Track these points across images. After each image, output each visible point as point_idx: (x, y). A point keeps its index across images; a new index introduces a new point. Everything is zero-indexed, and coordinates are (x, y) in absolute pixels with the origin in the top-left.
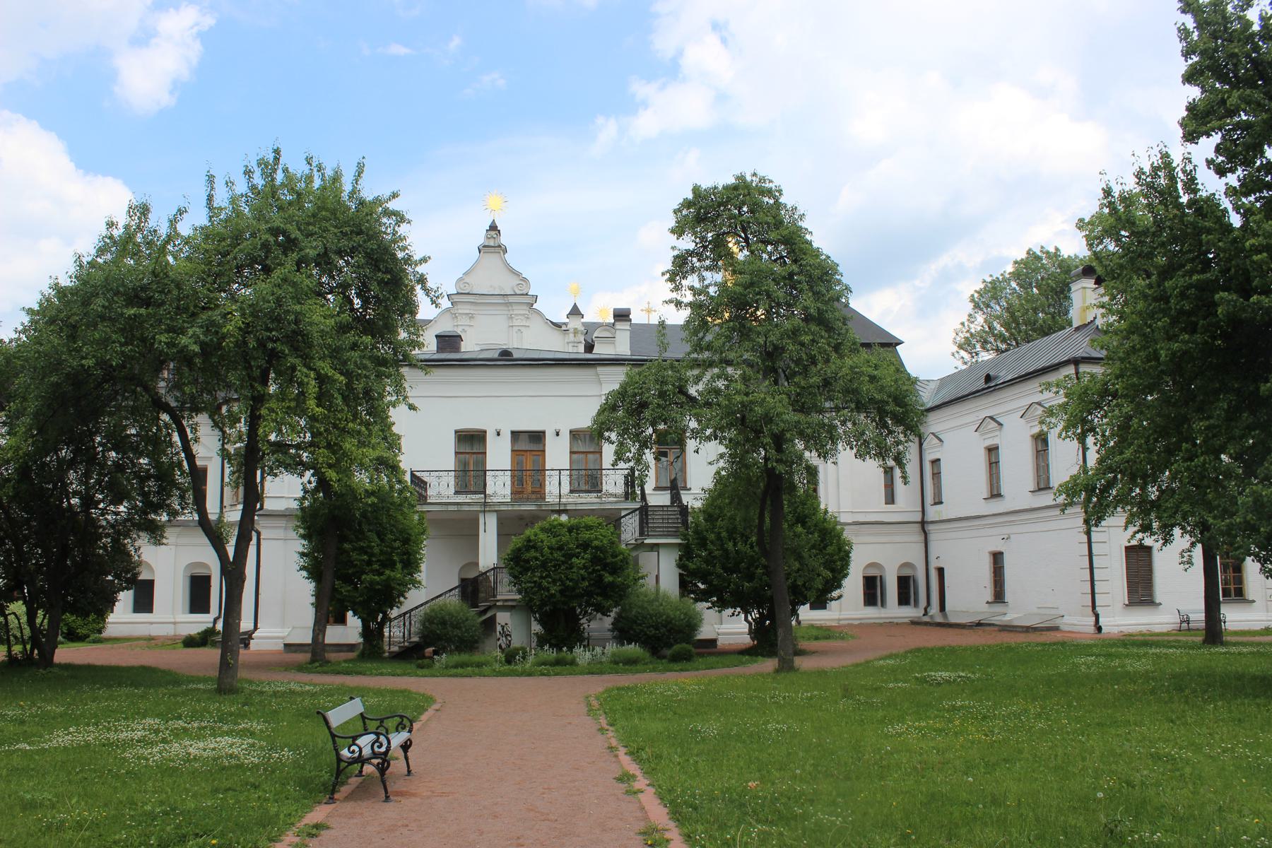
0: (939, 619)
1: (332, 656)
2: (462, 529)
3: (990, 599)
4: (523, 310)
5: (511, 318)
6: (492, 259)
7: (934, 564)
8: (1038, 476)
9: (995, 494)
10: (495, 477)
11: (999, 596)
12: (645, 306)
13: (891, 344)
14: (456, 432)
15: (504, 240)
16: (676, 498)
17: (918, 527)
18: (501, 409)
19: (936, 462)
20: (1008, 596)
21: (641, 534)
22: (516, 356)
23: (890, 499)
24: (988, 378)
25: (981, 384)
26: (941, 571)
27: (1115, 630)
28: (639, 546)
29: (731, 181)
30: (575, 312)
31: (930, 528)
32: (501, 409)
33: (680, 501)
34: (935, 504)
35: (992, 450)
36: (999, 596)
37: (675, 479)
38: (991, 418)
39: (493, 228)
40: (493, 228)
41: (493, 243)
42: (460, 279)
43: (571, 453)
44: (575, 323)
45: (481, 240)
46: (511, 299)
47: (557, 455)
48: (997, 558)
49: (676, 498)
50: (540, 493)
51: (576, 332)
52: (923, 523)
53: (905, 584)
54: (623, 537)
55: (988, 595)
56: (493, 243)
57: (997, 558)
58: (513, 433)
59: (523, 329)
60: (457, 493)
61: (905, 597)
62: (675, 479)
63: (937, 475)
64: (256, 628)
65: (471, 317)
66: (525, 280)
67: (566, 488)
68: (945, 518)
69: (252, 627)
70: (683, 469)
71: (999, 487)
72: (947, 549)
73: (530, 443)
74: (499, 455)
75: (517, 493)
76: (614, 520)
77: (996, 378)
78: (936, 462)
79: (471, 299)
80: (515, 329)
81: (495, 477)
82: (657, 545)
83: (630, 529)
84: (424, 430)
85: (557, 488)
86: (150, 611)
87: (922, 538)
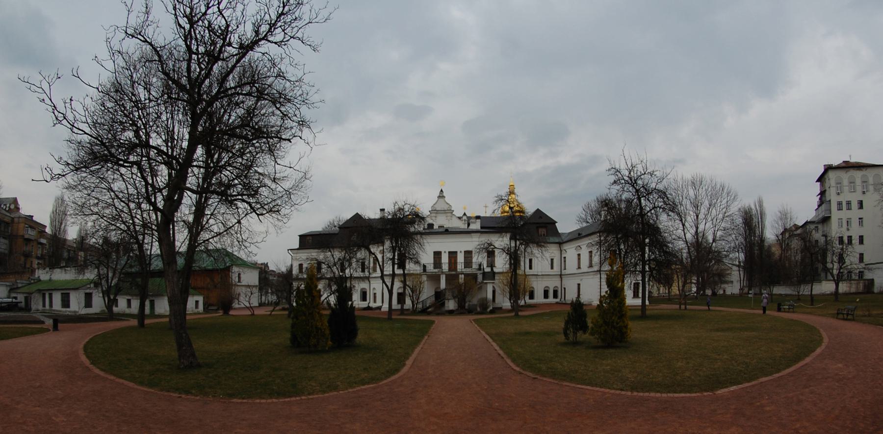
6: (441, 200)
13: (554, 223)
15: (445, 194)
16: (492, 269)
18: (445, 245)
23: (552, 268)
30: (465, 214)
35: (579, 255)
41: (441, 196)
47: (461, 258)
48: (579, 285)
49: (492, 269)
56: (441, 196)
57: (579, 285)
61: (555, 296)
74: (445, 259)
75: (450, 269)
83: (480, 278)
85: (460, 267)
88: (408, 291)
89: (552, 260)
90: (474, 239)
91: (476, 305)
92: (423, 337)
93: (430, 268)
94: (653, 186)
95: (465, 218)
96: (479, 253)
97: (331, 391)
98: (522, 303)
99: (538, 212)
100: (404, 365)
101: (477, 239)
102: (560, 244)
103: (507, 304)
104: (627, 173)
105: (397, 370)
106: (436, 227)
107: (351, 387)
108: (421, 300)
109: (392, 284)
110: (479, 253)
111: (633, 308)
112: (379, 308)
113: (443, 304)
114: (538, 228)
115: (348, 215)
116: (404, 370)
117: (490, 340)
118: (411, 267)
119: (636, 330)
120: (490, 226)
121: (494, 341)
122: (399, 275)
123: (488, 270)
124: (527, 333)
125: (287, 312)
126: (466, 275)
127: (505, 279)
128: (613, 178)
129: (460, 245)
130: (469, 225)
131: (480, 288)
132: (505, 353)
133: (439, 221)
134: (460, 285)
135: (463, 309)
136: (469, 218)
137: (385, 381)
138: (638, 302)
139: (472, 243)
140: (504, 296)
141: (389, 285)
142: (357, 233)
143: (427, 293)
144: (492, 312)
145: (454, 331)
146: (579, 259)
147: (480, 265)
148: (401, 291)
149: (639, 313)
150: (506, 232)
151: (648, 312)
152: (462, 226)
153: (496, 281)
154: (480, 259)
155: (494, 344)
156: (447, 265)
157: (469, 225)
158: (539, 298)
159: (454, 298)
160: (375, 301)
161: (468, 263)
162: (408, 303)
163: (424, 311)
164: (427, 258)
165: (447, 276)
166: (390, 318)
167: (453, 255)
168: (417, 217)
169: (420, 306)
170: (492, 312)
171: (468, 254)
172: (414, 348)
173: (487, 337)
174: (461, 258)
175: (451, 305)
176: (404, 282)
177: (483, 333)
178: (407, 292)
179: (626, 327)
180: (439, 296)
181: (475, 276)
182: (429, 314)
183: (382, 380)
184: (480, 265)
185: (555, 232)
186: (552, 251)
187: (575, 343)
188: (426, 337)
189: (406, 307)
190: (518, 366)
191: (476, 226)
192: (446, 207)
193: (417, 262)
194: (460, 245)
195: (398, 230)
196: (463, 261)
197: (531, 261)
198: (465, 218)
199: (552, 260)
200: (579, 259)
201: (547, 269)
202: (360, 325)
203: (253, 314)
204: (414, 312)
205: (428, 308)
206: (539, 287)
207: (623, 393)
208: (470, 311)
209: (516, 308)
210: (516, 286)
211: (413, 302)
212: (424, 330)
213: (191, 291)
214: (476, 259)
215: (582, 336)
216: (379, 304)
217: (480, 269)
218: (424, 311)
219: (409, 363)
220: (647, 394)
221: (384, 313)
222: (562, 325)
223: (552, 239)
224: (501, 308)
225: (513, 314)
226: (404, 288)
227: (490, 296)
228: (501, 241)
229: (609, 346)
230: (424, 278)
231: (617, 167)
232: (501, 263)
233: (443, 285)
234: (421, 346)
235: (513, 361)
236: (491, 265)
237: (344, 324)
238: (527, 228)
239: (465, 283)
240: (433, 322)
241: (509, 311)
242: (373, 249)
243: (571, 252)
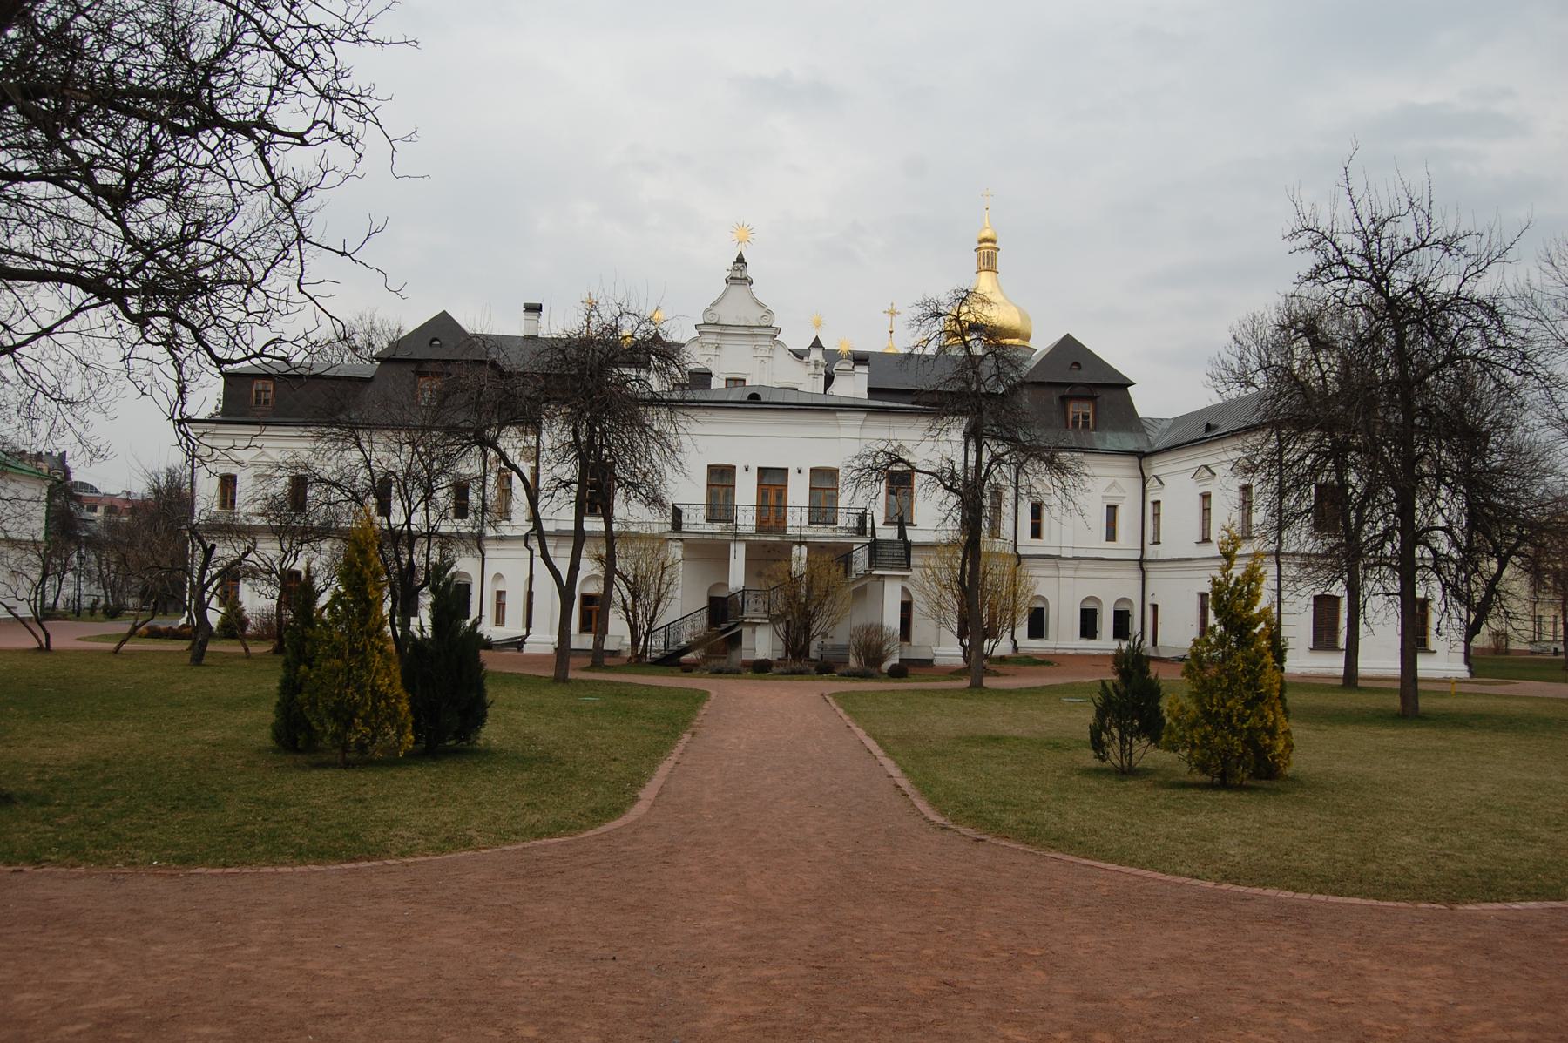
1: (608, 661)
2: (712, 553)
4: (766, 342)
6: (738, 290)
7: (1149, 600)
12: (887, 307)
13: (1123, 385)
15: (751, 272)
16: (902, 534)
18: (747, 445)
19: (1157, 503)
23: (1111, 535)
24: (1209, 428)
25: (1201, 433)
26: (1155, 607)
27: (1298, 671)
28: (867, 575)
30: (817, 343)
31: (1147, 566)
32: (747, 445)
35: (1206, 497)
39: (740, 259)
40: (740, 259)
41: (739, 275)
42: (708, 310)
46: (756, 331)
47: (798, 493)
49: (902, 534)
50: (780, 527)
53: (1122, 619)
56: (739, 275)
61: (1121, 630)
63: (1157, 516)
66: (769, 312)
67: (805, 522)
69: (524, 632)
73: (772, 480)
74: (746, 492)
75: (761, 528)
77: (1216, 427)
78: (1157, 503)
79: (718, 329)
83: (861, 559)
85: (796, 520)
88: (621, 591)
89: (1112, 510)
90: (844, 432)
91: (847, 648)
92: (676, 736)
93: (696, 519)
94: (1447, 286)
95: (816, 355)
96: (858, 482)
97: (455, 848)
98: (1003, 647)
99: (1068, 343)
100: (635, 799)
101: (855, 433)
102: (1141, 456)
103: (949, 650)
104: (1359, 246)
105: (618, 811)
106: (717, 383)
107: (506, 841)
108: (660, 622)
109: (574, 568)
110: (858, 482)
111: (1311, 684)
112: (517, 644)
113: (736, 641)
114: (1064, 400)
115: (411, 318)
116: (636, 812)
117: (878, 752)
118: (629, 512)
119: (1308, 750)
120: (900, 390)
121: (890, 754)
122: (594, 536)
123: (888, 534)
124: (997, 740)
125: (184, 645)
126: (816, 548)
127: (948, 567)
128: (1310, 261)
129: (799, 448)
130: (829, 380)
131: (860, 593)
132: (916, 784)
133: (727, 363)
134: (795, 581)
135: (800, 659)
136: (832, 356)
137: (591, 833)
138: (1333, 664)
139: (843, 444)
140: (942, 622)
141: (563, 567)
142: (449, 386)
143: (682, 604)
144: (899, 672)
145: (766, 727)
146: (1206, 511)
147: (862, 519)
148: (594, 589)
149: (1395, 703)
150: (961, 413)
151: (1423, 703)
152: (809, 383)
153: (915, 574)
154: (862, 499)
155: (889, 764)
156: (753, 512)
157: (829, 380)
158: (1064, 636)
159: (774, 620)
160: (499, 620)
161: (822, 511)
162: (618, 631)
163: (671, 660)
164: (687, 489)
165: (750, 547)
166: (561, 678)
168: (655, 350)
169: (657, 643)
170: (899, 672)
171: (824, 479)
172: (654, 765)
173: (871, 743)
174: (798, 493)
175: (762, 643)
176: (609, 561)
177: (861, 733)
178: (616, 595)
179: (1272, 732)
180: (722, 613)
181: (843, 555)
182: (688, 669)
183: (582, 828)
184: (862, 519)
185: (1126, 418)
186: (1103, 481)
187: (1127, 772)
188: (687, 737)
189: (609, 644)
190: (943, 813)
191: (852, 386)
193: (654, 500)
194: (799, 448)
195: (599, 388)
197: (1037, 511)
198: (816, 355)
199: (1112, 510)
200: (1206, 511)
201: (1095, 542)
202: (491, 692)
203: (45, 649)
204: (638, 660)
205: (685, 650)
206: (1064, 598)
207: (1195, 882)
208: (826, 668)
209: (977, 666)
210: (978, 600)
211: (633, 628)
212: (678, 718)
213: (1398, 685)
214: (849, 500)
215: (1146, 753)
216: (513, 627)
217: (861, 530)
218: (671, 660)
219: (648, 794)
220: (1257, 890)
221: (537, 659)
222: (1088, 716)
223: (1112, 440)
224: (928, 663)
225: (965, 683)
226: (609, 582)
227: (892, 620)
228: (936, 446)
229: (1224, 782)
230: (676, 551)
231: (1324, 225)
232: (933, 516)
233: (737, 577)
234: (674, 758)
235: (934, 802)
236: (901, 520)
237: (448, 687)
238: (1022, 402)
239: (811, 574)
240: (703, 696)
241: (956, 673)
242: (512, 443)
243: (1178, 482)
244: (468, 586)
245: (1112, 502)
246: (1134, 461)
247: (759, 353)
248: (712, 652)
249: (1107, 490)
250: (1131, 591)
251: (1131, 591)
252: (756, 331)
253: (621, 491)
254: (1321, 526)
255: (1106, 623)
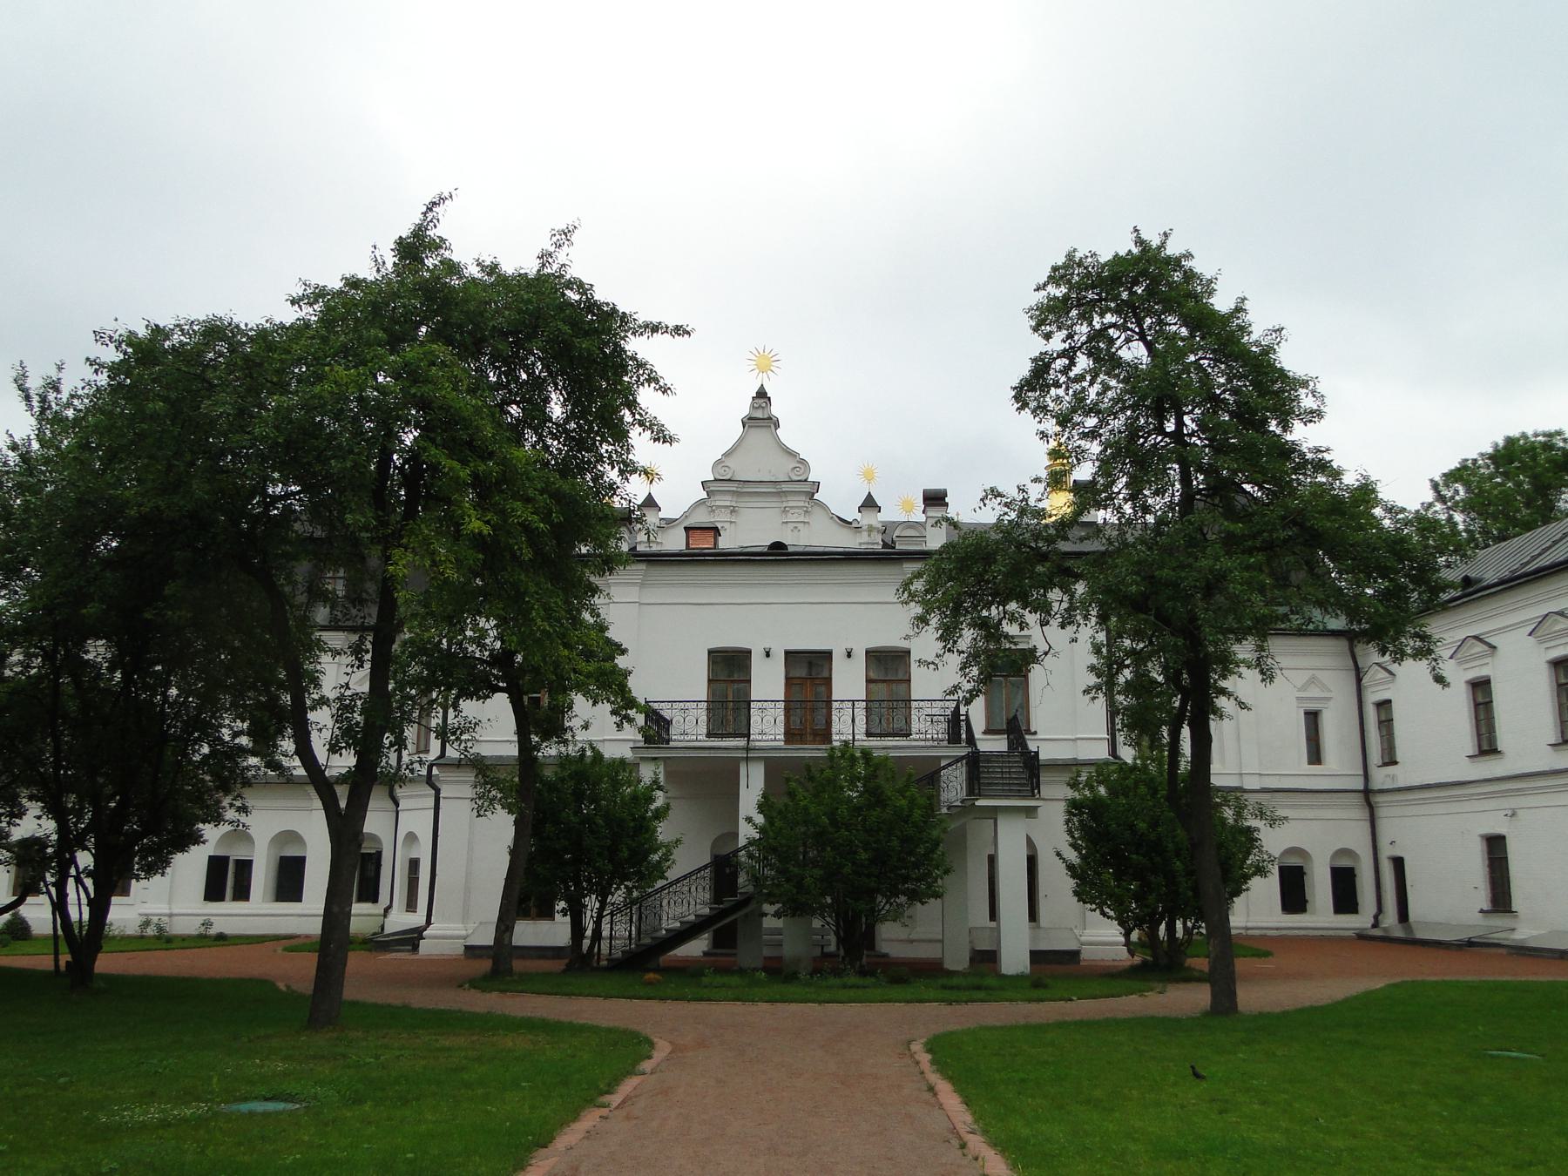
0: (1398, 933)
1: (518, 965)
2: (711, 780)
3: (1486, 906)
4: (801, 502)
5: (785, 511)
6: (759, 435)
7: (1386, 852)
8: (1479, 735)
9: (1487, 746)
10: (762, 710)
11: (1501, 898)
14: (710, 652)
15: (776, 410)
17: (1358, 799)
20: (1517, 904)
21: (970, 791)
22: (791, 549)
23: (1315, 756)
26: (1398, 863)
28: (966, 809)
29: (1125, 246)
31: (1379, 799)
33: (1025, 747)
34: (1385, 764)
36: (1501, 898)
37: (1015, 717)
38: (1476, 637)
39: (762, 394)
40: (762, 394)
41: (760, 417)
43: (869, 681)
44: (868, 519)
45: (745, 410)
48: (1496, 847)
51: (871, 529)
52: (1368, 794)
54: (944, 796)
55: (1482, 899)
56: (760, 417)
57: (1496, 847)
58: (787, 653)
59: (800, 526)
60: (709, 735)
61: (1345, 899)
62: (1015, 717)
63: (1386, 724)
64: (429, 922)
65: (733, 511)
66: (803, 462)
68: (1401, 784)
70: (1026, 705)
71: (1492, 739)
72: (1404, 830)
74: (768, 682)
75: (791, 735)
76: (930, 775)
77: (1479, 581)
78: (1384, 705)
79: (732, 487)
80: (791, 526)
81: (762, 710)
82: (996, 808)
83: (954, 786)
84: (660, 638)
85: (848, 726)
86: (300, 900)
87: (1367, 815)
89: (1313, 718)
93: (690, 728)
112: (412, 938)
165: (775, 768)
167: (809, 670)
171: (888, 665)
174: (849, 682)
192: (780, 469)
193: (624, 703)
196: (779, 692)
199: (1313, 718)
201: (1292, 766)
244: (379, 854)
245: (1313, 706)
246: (1342, 645)
247: (791, 518)
248: (725, 940)
249: (1303, 688)
250: (1354, 837)
251: (1354, 837)
252: (785, 487)
253: (832, 948)
254: (160, 1120)
255: (1320, 888)
